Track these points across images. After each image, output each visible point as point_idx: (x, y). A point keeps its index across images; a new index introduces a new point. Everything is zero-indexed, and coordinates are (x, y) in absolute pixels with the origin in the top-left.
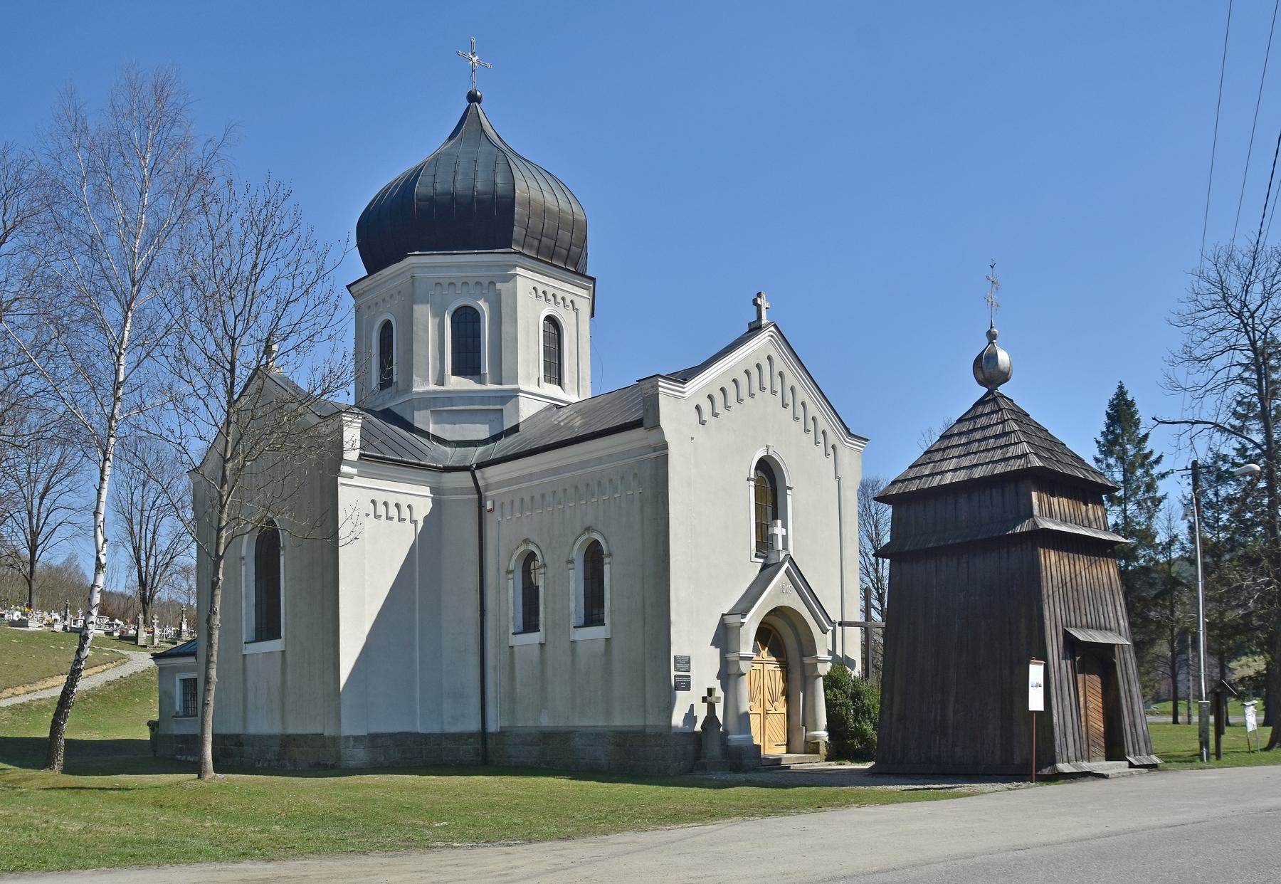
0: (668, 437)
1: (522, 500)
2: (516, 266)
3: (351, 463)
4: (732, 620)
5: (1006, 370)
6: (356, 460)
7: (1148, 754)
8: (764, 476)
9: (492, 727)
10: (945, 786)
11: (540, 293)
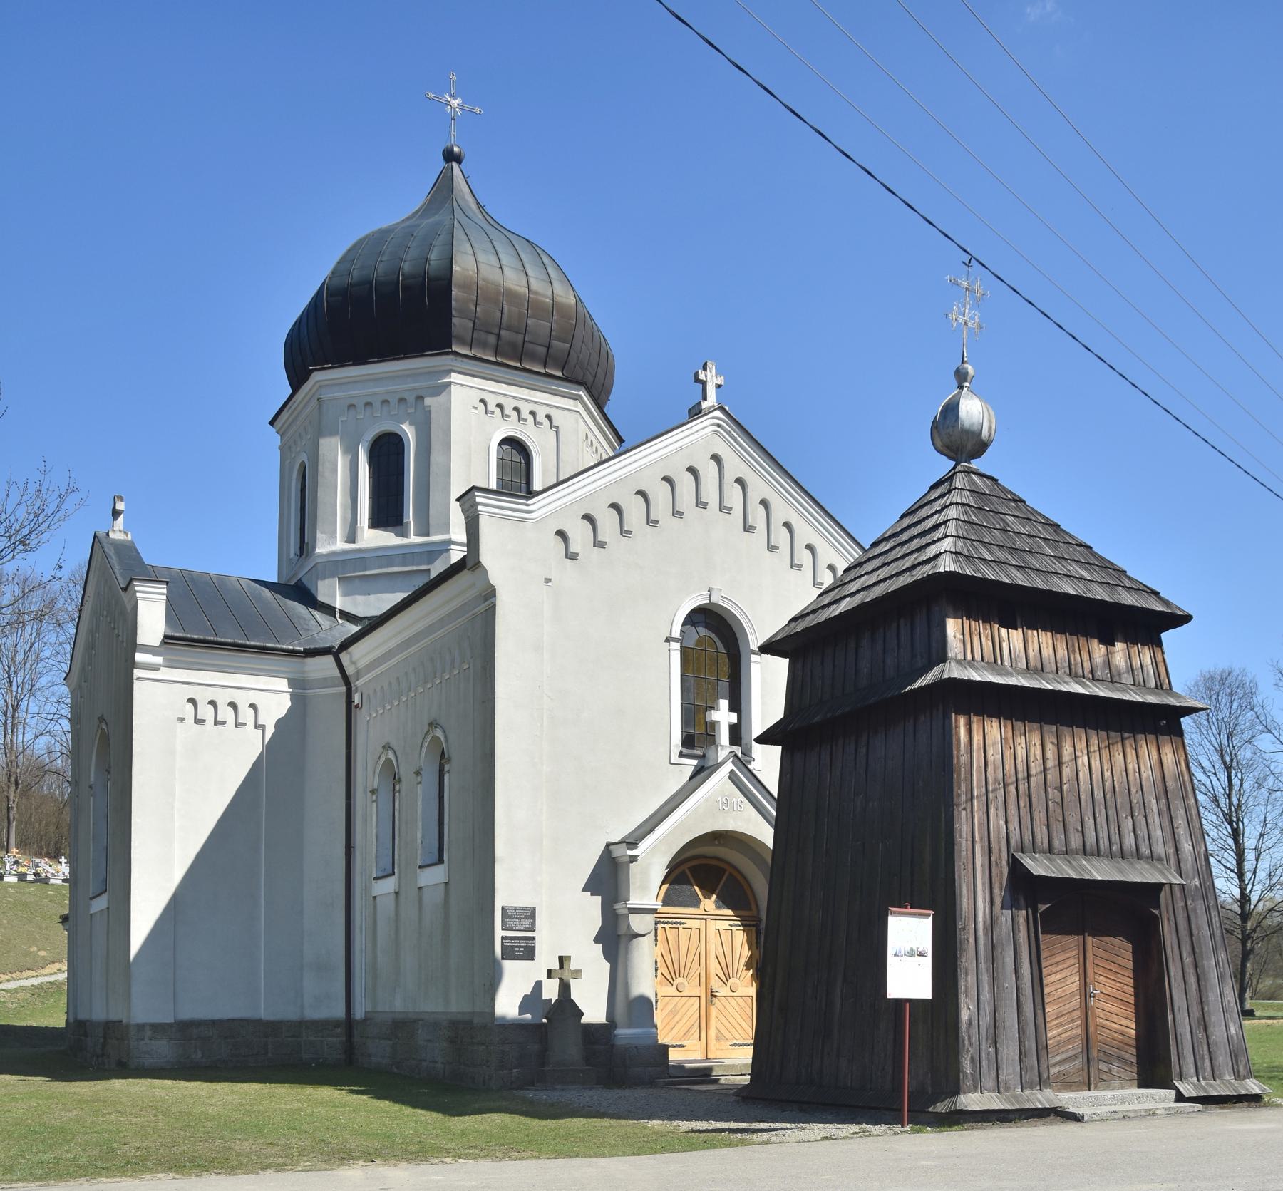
0: (494, 578)
1: (382, 687)
2: (448, 372)
3: (149, 649)
4: (619, 852)
5: (975, 428)
6: (158, 645)
7: (1237, 1076)
8: (713, 636)
9: (359, 1013)
10: (725, 1125)
11: (492, 406)
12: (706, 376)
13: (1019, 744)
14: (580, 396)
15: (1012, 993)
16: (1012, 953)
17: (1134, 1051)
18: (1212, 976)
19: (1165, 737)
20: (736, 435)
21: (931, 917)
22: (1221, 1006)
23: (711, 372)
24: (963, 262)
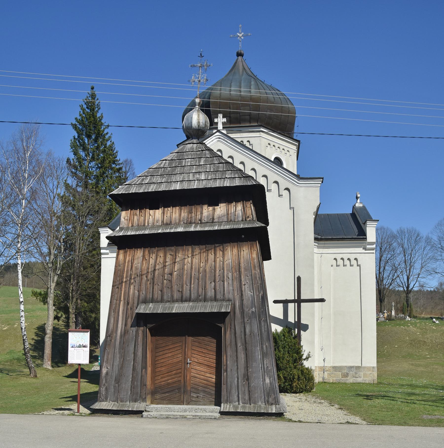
12: (218, 120)
13: (151, 258)
14: (261, 130)
15: (131, 362)
16: (133, 346)
17: (214, 389)
18: (257, 354)
19: (197, 246)
20: (226, 140)
21: (89, 332)
22: (261, 368)
23: (220, 118)
24: (199, 56)
